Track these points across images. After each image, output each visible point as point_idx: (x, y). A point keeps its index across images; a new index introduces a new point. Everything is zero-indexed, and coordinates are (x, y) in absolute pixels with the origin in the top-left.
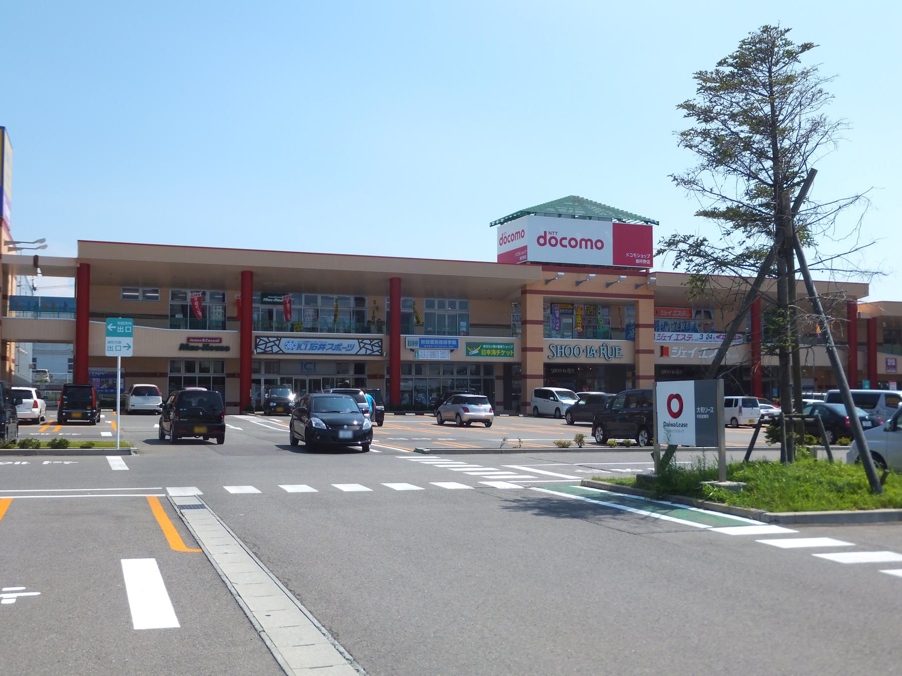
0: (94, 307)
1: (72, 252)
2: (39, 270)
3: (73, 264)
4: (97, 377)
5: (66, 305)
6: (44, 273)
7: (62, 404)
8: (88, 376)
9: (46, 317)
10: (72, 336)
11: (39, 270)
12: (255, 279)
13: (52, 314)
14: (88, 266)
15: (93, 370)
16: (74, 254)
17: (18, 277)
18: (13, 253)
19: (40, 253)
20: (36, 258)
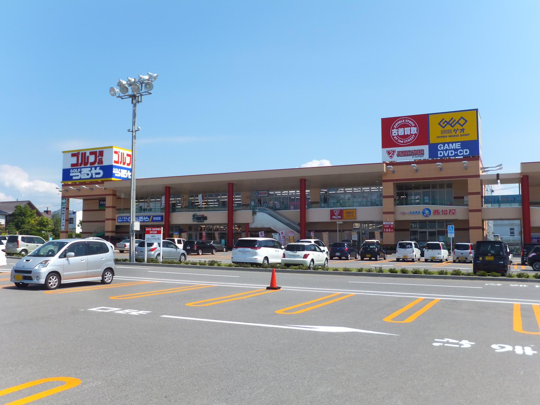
0: (532, 199)
1: (517, 170)
2: (499, 181)
3: (518, 176)
4: (535, 238)
5: (514, 199)
6: (502, 183)
7: (523, 253)
8: (531, 238)
9: (503, 206)
10: (520, 215)
11: (499, 181)
12: (171, 190)
13: (508, 204)
14: (527, 176)
15: (533, 235)
16: (519, 171)
17: (486, 186)
18: (484, 174)
19: (500, 172)
20: (498, 175)
